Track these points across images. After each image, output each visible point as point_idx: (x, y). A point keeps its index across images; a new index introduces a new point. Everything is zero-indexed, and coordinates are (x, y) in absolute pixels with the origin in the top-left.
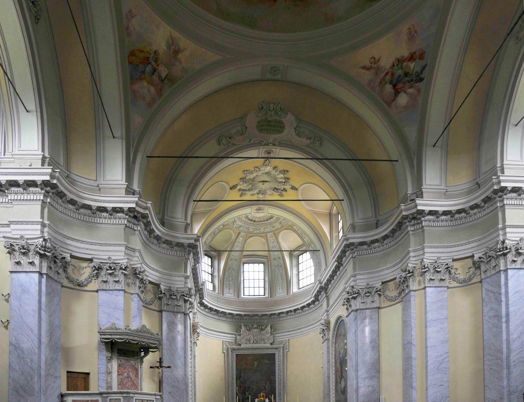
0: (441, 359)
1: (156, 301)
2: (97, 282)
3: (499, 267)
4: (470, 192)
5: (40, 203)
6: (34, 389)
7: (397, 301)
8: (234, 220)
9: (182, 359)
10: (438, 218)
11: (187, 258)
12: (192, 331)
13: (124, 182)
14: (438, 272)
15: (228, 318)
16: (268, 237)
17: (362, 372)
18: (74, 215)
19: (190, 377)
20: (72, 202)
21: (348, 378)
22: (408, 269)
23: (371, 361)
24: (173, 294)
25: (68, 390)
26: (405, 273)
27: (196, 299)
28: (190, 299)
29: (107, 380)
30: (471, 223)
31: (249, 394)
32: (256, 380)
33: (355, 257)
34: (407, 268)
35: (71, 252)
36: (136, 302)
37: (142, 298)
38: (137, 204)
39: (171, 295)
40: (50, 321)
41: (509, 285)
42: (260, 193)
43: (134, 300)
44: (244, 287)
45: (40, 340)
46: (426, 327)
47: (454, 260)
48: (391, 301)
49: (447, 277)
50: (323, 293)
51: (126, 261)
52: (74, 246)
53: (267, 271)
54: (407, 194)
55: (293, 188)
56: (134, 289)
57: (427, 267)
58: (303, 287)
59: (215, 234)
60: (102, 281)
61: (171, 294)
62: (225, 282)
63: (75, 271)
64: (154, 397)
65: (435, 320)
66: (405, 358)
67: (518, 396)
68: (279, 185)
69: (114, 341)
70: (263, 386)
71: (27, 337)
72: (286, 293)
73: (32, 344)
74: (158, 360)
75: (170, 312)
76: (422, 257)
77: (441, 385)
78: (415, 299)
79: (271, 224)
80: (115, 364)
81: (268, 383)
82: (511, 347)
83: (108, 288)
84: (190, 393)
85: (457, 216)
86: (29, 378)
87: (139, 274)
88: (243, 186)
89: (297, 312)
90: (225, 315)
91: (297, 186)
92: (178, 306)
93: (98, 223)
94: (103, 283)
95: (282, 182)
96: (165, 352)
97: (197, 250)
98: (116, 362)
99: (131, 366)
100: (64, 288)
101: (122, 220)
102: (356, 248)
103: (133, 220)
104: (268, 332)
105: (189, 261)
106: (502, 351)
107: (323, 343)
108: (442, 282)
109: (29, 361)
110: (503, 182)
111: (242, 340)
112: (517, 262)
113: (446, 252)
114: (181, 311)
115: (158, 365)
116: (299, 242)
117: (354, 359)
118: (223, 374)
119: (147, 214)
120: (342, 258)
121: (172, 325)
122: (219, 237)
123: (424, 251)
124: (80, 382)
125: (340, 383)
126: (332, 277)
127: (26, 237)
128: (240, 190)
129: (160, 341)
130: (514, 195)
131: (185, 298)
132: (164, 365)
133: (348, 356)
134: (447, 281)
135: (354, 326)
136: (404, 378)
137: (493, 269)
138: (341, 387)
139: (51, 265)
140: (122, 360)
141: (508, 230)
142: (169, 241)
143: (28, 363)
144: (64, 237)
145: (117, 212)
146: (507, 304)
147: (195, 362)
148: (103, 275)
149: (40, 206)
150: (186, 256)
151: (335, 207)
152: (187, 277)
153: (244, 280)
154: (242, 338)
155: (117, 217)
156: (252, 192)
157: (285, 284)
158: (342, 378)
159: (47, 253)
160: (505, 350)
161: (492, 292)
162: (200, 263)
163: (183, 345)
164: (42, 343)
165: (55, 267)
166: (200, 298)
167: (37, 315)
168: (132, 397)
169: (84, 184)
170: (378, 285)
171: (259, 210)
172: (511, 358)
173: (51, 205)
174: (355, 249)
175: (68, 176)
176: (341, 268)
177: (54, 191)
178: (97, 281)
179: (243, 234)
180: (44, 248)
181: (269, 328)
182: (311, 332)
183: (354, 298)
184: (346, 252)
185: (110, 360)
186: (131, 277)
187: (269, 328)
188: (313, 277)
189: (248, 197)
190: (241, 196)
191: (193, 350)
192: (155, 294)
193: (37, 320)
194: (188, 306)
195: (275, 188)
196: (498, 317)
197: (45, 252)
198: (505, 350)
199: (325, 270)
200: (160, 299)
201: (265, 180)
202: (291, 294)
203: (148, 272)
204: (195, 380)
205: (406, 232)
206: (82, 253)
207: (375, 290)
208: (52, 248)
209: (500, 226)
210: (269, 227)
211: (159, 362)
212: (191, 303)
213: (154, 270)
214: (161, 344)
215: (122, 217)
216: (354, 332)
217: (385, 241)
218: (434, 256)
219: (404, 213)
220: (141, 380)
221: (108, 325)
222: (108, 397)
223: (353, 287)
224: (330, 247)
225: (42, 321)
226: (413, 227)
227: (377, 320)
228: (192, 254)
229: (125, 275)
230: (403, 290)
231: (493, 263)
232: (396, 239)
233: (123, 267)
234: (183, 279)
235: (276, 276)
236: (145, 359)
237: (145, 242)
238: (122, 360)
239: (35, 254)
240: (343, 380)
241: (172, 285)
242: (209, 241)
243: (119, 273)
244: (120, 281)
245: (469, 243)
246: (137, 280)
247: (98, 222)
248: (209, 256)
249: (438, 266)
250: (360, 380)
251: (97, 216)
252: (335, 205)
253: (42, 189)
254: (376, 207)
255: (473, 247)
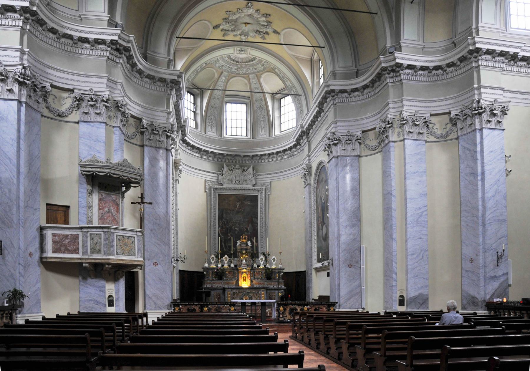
0: (420, 211)
1: (138, 135)
2: (78, 114)
3: (475, 126)
4: (447, 50)
5: (20, 30)
6: (12, 220)
7: (377, 151)
8: (216, 59)
9: (164, 196)
10: (416, 72)
11: (169, 93)
12: (174, 168)
13: (106, 14)
14: (416, 125)
15: (210, 157)
16: (251, 78)
17: (343, 219)
18: (55, 44)
19: (172, 215)
20: (53, 31)
21: (329, 225)
22: (387, 120)
23: (353, 209)
24: (156, 129)
25: (47, 223)
26: (385, 124)
27: (178, 135)
28: (172, 135)
29: (87, 214)
30: (447, 81)
31: (231, 236)
32: (238, 222)
33: (336, 104)
34: (386, 118)
35: (51, 81)
36: (118, 136)
37: (124, 132)
38: (119, 37)
39: (153, 130)
40: (30, 151)
41: (484, 144)
42: (242, 34)
43: (116, 133)
44: (226, 127)
45: (19, 170)
46: (405, 179)
47: (432, 115)
48: (372, 150)
49: (424, 130)
50: (304, 137)
51: (108, 93)
52: (55, 76)
53: (249, 112)
54: (386, 47)
55: (275, 32)
56: (117, 122)
57: (406, 120)
58: (285, 130)
59: (197, 72)
60: (83, 112)
61: (153, 129)
62: (207, 121)
63: (56, 100)
64: (135, 233)
65: (414, 173)
66: (385, 208)
67: (492, 254)
68: (262, 27)
69: (94, 174)
70: (246, 228)
71: (5, 166)
72: (268, 135)
73: (10, 173)
74: (140, 196)
75: (152, 147)
76: (401, 109)
77: (420, 238)
78: (395, 151)
79: (253, 65)
80: (95, 198)
81: (250, 225)
82: (486, 205)
83: (89, 120)
84: (172, 231)
85: (434, 72)
86: (7, 209)
87: (121, 107)
88: (226, 26)
89: (279, 154)
90: (207, 154)
91: (279, 30)
92: (161, 141)
93: (80, 54)
94: (84, 114)
95: (264, 25)
96: (146, 187)
97: (179, 86)
98: (97, 197)
99: (113, 201)
100: (44, 118)
101: (105, 52)
102: (337, 95)
103: (115, 53)
104: (250, 174)
105: (171, 97)
106: (478, 209)
107: (305, 188)
108: (420, 135)
109: (7, 191)
110: (478, 43)
111: (225, 180)
112: (492, 123)
113: (424, 107)
114: (163, 147)
115: (139, 200)
116: (282, 86)
117: (335, 205)
118: (205, 213)
119: (130, 47)
120: (323, 104)
121: (154, 161)
122: (202, 76)
123: (403, 103)
124: (60, 215)
125: (322, 230)
126: (313, 122)
127: (4, 63)
128: (222, 30)
129: (142, 176)
130: (488, 57)
131: (168, 133)
132: (146, 200)
133: (329, 202)
134: (425, 135)
135: (335, 173)
136: (385, 228)
137: (469, 127)
138: (322, 233)
139: (30, 93)
140: (103, 194)
141: (483, 90)
142: (152, 76)
143: (6, 193)
144: (45, 66)
145: (100, 44)
146: (483, 163)
147: (176, 200)
148: (85, 107)
149: (18, 33)
150: (168, 91)
151: (316, 54)
152: (169, 113)
153: (226, 119)
154: (224, 178)
155: (99, 48)
156: (235, 33)
157: (267, 126)
158: (324, 225)
159: (26, 81)
160: (480, 207)
161: (468, 149)
162: (182, 99)
163: (165, 181)
164: (21, 173)
165: (34, 96)
166: (182, 135)
167: (15, 145)
168: (113, 233)
169: (66, 13)
170: (359, 134)
171: (241, 51)
172: (487, 215)
173: (31, 32)
174: (336, 96)
175: (48, 4)
176: (322, 114)
177: (34, 18)
178: (78, 112)
179: (225, 73)
180: (24, 75)
181: (251, 169)
182: (293, 176)
183: (335, 145)
184: (327, 99)
185: (90, 193)
186: (113, 110)
187: (251, 169)
188: (295, 121)
189: (230, 37)
190: (224, 36)
191: (175, 187)
192: (137, 128)
193: (15, 149)
194: (170, 142)
195: (258, 31)
196: (474, 174)
197: (25, 80)
198: (480, 207)
199: (306, 114)
200: (142, 133)
201: (248, 22)
202: (273, 136)
203: (130, 106)
204: (176, 219)
205: (385, 83)
206: (63, 83)
207: (355, 138)
208: (31, 76)
209: (476, 86)
210: (251, 69)
211: (140, 198)
212: (173, 140)
213: (136, 103)
214: (142, 180)
215: (104, 48)
216: (335, 178)
217: (365, 91)
218: (413, 110)
219: (383, 65)
220: (122, 216)
221: (89, 158)
222: (88, 231)
223: (334, 133)
224: (311, 92)
225: (21, 151)
226: (392, 80)
227: (357, 168)
228: (174, 90)
229: (106, 107)
230: (382, 140)
231: (469, 121)
232: (375, 89)
233: (105, 100)
234: (165, 114)
235: (258, 118)
236: (126, 194)
237: (127, 75)
238: (103, 194)
239: (14, 81)
240: (324, 226)
241: (154, 121)
242: (192, 78)
243: (100, 105)
244: (102, 113)
245: (446, 100)
246: (119, 113)
247: (80, 52)
248: (191, 94)
249: (416, 120)
250: (341, 227)
251: (79, 46)
252: (316, 51)
253: (21, 15)
254: (356, 56)
255: (450, 104)
